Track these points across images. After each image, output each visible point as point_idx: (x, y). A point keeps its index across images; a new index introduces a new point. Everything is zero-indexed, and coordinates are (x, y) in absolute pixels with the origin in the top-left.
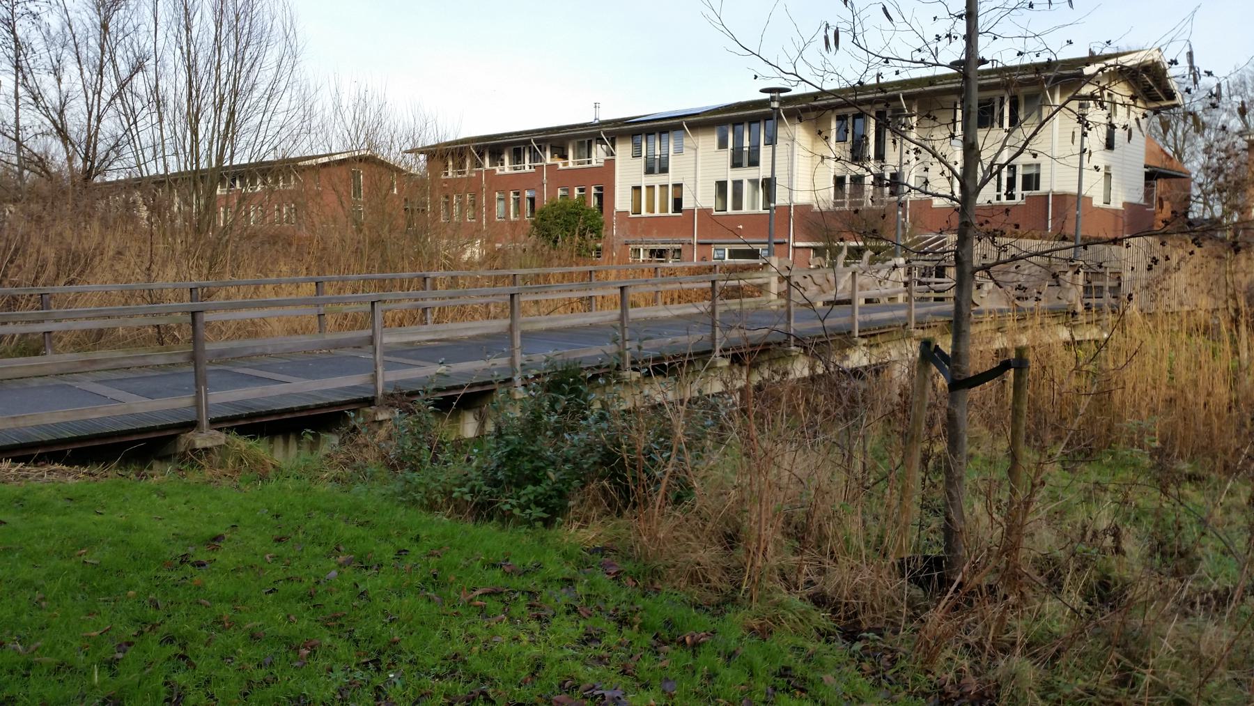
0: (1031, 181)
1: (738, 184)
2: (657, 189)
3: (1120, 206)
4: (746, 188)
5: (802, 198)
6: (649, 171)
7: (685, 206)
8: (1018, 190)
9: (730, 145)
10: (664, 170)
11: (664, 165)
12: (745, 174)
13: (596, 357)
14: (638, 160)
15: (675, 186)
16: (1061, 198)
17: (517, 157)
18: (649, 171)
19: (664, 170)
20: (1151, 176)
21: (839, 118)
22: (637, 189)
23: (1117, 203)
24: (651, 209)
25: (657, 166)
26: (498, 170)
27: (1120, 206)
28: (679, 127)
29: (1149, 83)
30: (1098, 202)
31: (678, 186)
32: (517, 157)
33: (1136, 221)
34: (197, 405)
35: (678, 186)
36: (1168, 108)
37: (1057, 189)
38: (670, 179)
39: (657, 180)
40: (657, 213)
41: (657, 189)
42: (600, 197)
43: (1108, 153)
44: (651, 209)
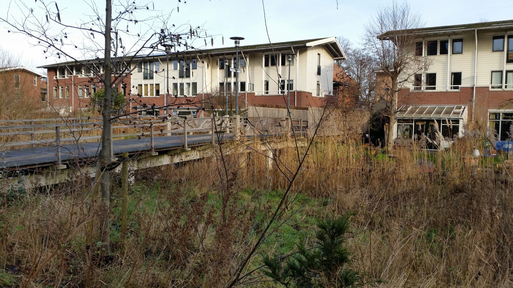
0: (290, 86)
1: (146, 85)
2: (149, 86)
3: (323, 96)
4: (185, 86)
5: (208, 90)
6: (145, 78)
7: (160, 93)
8: (286, 90)
9: (178, 69)
10: (152, 78)
11: (151, 76)
12: (185, 81)
13: (140, 147)
14: (140, 73)
15: (156, 85)
16: (300, 93)
17: (88, 71)
18: (145, 78)
19: (152, 78)
20: (336, 85)
21: (220, 60)
22: (140, 85)
23: (322, 95)
24: (146, 94)
25: (148, 76)
26: (79, 76)
27: (323, 96)
28: (157, 60)
29: (332, 49)
30: (314, 94)
31: (158, 85)
32: (79, 71)
33: (329, 103)
34: (105, 140)
35: (158, 85)
36: (341, 59)
37: (298, 89)
38: (154, 81)
39: (149, 82)
40: (149, 96)
41: (149, 86)
42: (124, 88)
43: (319, 76)
44: (146, 94)
